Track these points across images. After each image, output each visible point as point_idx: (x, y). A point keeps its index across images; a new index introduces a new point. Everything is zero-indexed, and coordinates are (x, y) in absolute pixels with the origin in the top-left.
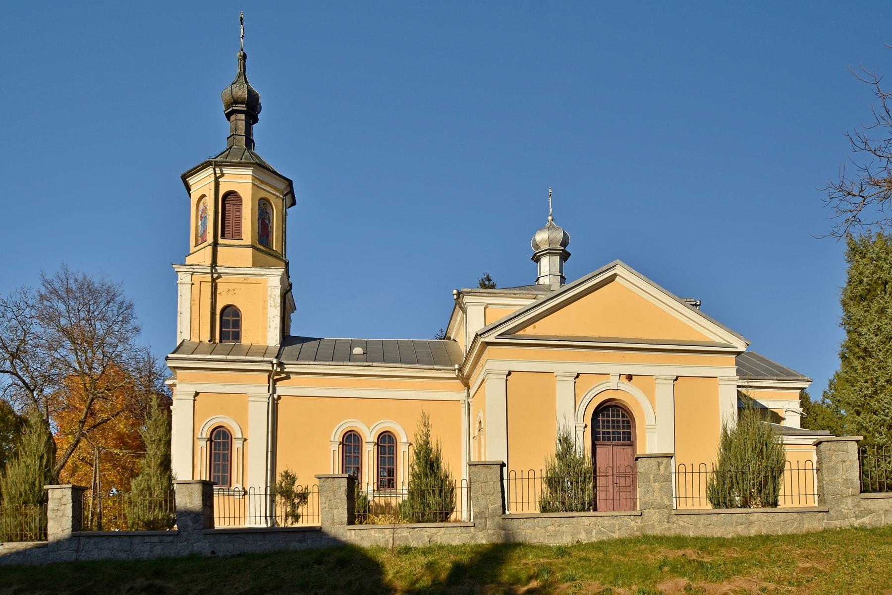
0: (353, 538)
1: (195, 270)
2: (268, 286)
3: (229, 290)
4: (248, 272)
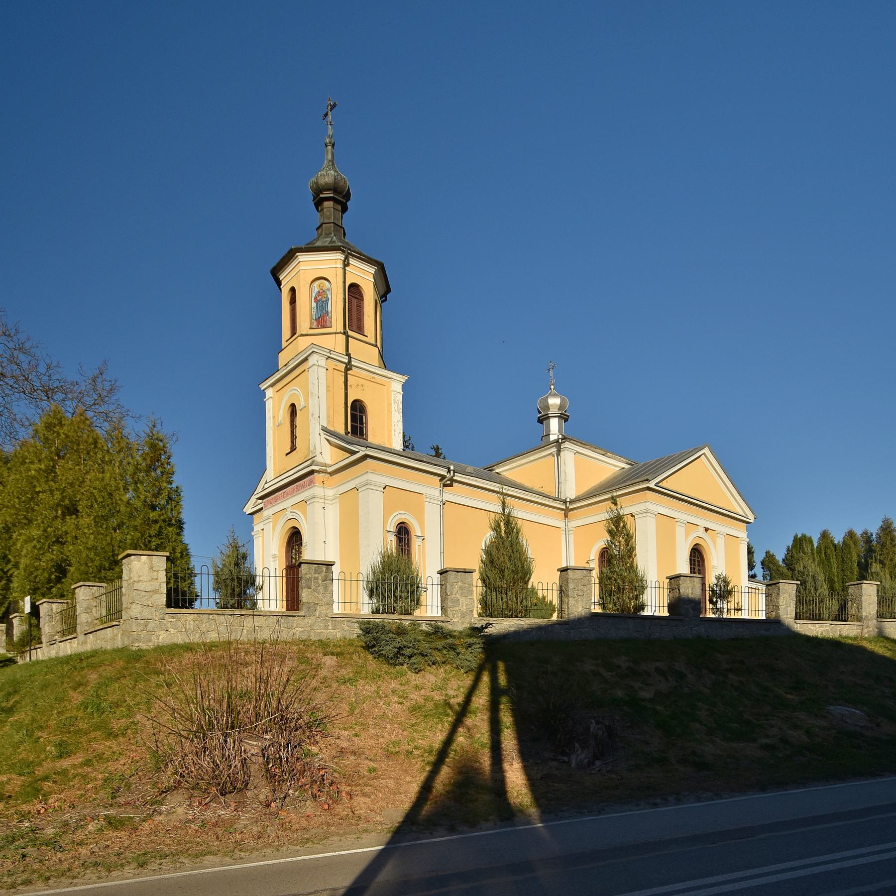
0: (799, 629)
1: (331, 356)
2: (392, 389)
3: (358, 385)
4: (378, 372)
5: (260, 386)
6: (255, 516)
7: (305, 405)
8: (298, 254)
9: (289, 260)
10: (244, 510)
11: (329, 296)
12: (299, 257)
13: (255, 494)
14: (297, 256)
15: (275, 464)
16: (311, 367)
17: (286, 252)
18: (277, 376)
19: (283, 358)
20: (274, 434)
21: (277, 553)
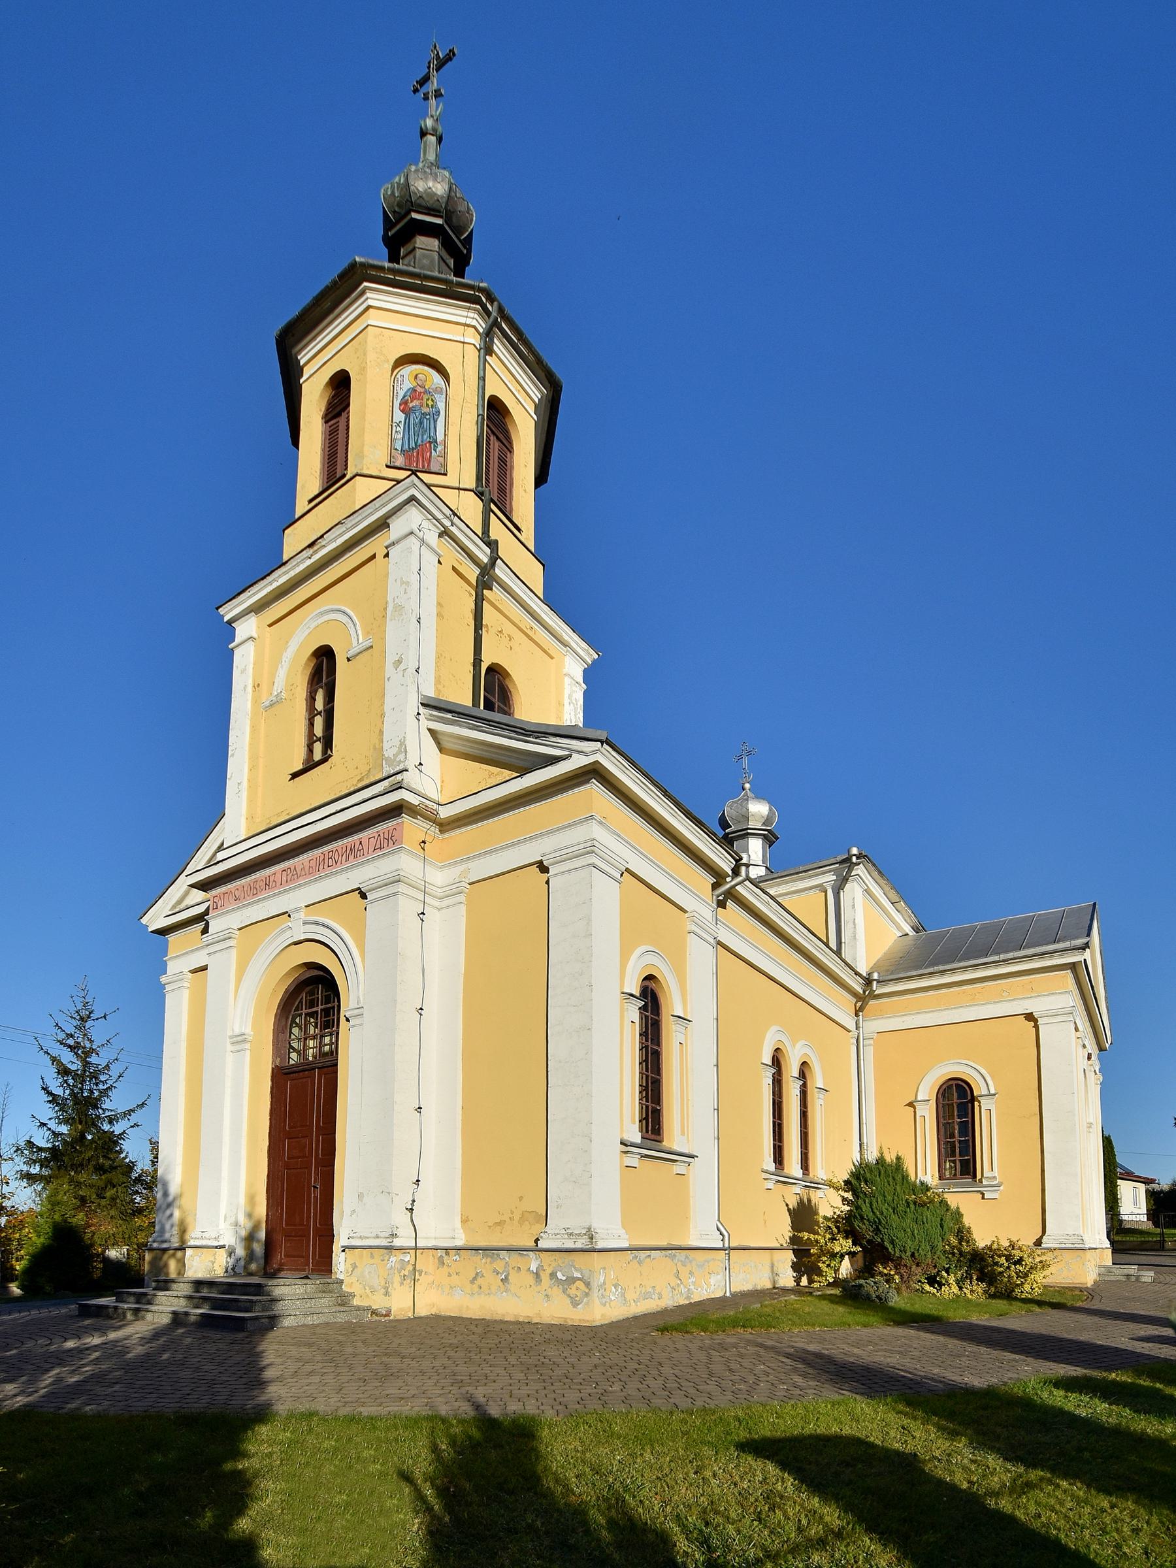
2: (565, 671)
3: (501, 632)
5: (222, 611)
6: (172, 938)
7: (368, 644)
8: (366, 284)
9: (331, 310)
10: (144, 921)
11: (441, 406)
12: (369, 294)
13: (187, 872)
14: (363, 293)
15: (251, 800)
16: (398, 541)
17: (335, 275)
18: (280, 578)
19: (294, 540)
20: (254, 729)
21: (248, 1030)
